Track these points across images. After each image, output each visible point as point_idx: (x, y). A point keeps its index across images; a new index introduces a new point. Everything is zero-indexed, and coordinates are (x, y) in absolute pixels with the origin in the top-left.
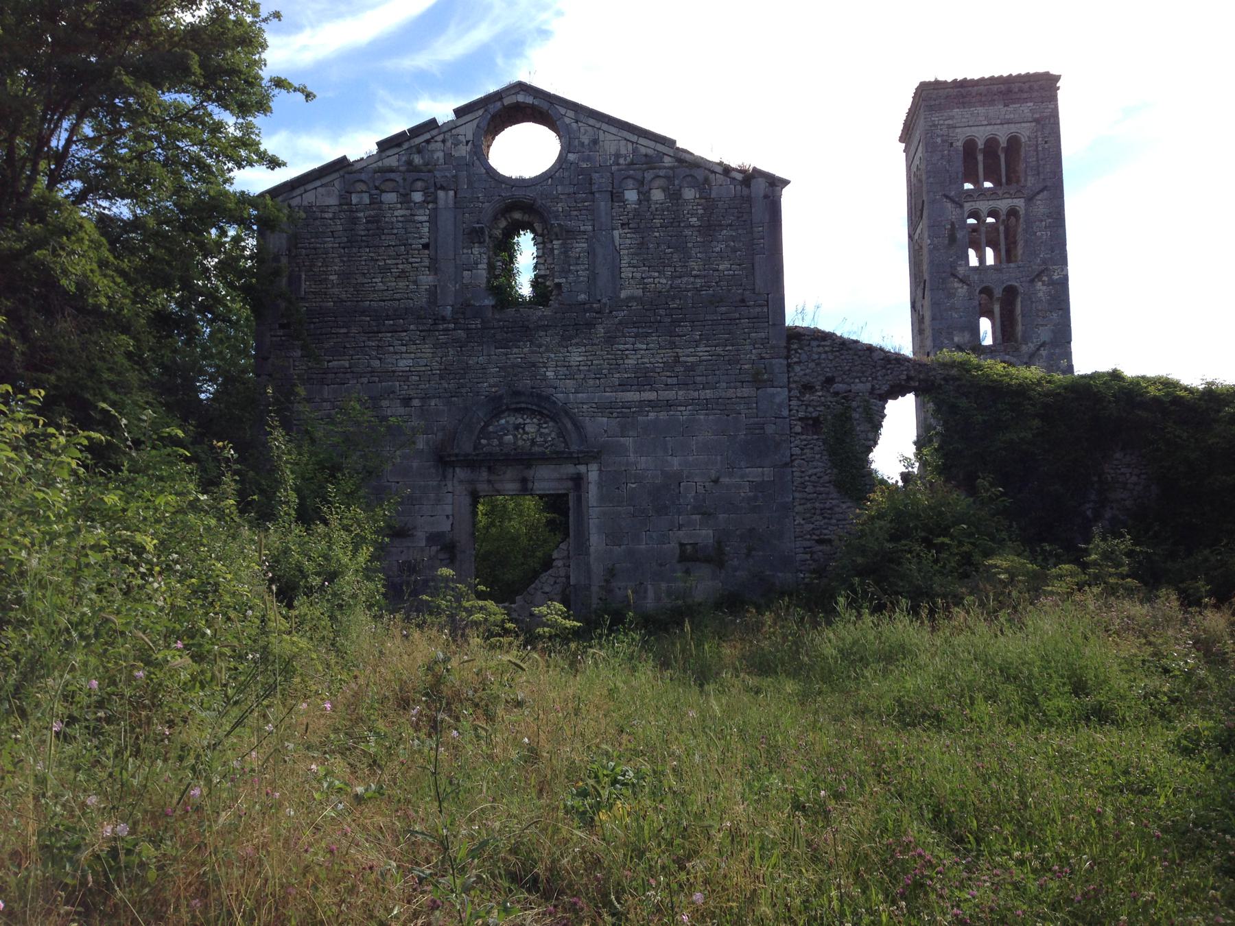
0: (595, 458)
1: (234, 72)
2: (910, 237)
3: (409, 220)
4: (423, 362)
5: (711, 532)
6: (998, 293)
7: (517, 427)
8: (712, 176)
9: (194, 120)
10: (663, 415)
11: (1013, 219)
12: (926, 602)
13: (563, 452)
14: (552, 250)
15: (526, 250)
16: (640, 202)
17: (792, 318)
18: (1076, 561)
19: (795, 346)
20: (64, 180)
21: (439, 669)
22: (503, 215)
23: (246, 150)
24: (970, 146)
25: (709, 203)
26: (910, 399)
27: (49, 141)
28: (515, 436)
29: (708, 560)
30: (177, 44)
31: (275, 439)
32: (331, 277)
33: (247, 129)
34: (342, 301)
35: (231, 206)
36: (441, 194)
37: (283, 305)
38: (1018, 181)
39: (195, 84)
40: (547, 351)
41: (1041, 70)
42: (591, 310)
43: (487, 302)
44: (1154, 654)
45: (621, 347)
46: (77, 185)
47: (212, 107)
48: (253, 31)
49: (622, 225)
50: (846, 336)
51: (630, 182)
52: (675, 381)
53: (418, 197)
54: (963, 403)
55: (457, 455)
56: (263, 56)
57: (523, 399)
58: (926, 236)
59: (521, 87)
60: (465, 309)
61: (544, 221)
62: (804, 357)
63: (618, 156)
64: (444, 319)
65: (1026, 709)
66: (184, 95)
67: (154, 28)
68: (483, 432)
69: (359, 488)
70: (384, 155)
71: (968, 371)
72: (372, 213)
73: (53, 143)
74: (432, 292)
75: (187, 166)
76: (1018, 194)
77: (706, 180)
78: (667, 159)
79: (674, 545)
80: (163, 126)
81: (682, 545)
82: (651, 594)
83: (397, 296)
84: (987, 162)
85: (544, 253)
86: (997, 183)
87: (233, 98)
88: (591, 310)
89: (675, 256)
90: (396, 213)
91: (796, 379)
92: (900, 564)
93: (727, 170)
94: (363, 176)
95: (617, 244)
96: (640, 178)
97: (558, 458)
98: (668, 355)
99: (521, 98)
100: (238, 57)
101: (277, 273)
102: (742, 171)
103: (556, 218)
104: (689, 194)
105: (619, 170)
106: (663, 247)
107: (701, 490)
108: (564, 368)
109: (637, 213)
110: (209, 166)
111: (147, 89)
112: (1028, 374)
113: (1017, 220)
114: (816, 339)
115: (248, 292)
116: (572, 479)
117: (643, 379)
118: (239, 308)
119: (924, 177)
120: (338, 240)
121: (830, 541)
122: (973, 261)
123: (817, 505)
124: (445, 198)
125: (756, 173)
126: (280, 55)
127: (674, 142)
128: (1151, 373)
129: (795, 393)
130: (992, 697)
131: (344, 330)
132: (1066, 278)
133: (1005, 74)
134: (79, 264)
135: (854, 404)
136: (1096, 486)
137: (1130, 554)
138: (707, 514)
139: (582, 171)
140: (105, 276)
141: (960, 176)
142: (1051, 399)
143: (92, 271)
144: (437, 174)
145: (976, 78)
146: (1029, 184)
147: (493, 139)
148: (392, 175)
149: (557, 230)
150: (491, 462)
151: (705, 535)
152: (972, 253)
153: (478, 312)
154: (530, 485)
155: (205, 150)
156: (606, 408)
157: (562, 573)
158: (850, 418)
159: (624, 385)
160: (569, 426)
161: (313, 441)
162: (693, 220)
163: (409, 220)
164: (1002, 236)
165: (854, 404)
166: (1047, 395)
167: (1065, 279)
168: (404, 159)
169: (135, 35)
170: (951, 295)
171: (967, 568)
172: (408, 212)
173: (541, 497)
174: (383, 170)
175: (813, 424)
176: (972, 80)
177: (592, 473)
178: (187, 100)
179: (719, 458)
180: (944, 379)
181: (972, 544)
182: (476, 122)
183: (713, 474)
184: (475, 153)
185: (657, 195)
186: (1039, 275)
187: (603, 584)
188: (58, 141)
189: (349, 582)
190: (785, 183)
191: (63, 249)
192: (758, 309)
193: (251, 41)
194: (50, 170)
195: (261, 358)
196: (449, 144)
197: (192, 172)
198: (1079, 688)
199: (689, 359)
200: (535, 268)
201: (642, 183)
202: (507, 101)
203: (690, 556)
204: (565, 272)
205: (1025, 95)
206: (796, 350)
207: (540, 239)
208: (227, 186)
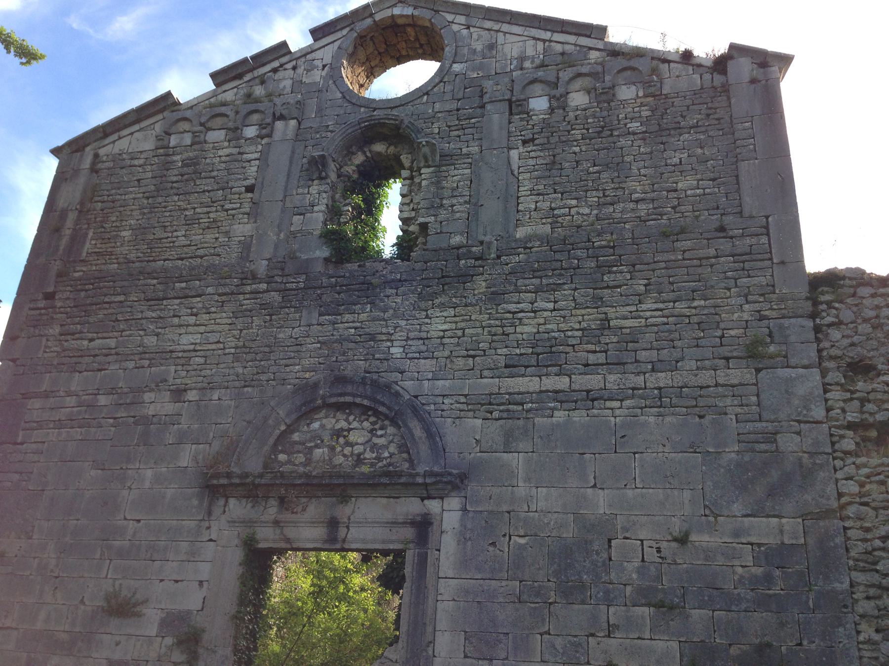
0: (456, 487)
4: (213, 338)
5: (675, 645)
7: (338, 433)
10: (579, 417)
13: (400, 475)
16: (552, 110)
17: (822, 251)
19: (827, 297)
22: (361, 149)
28: (332, 449)
32: (124, 234)
36: (279, 125)
40: (395, 316)
42: (469, 256)
45: (512, 307)
51: (538, 88)
53: (251, 132)
62: (847, 315)
64: (254, 277)
74: (246, 246)
83: (201, 252)
85: (410, 191)
88: (469, 256)
90: (220, 153)
91: (834, 352)
94: (188, 114)
95: (515, 167)
96: (552, 78)
98: (590, 318)
104: (626, 93)
106: (585, 165)
107: (651, 555)
116: (413, 523)
117: (546, 355)
120: (142, 190)
129: (836, 376)
131: (122, 298)
144: (278, 101)
148: (223, 110)
149: (426, 150)
153: (304, 268)
154: (342, 532)
156: (484, 405)
159: (512, 367)
160: (418, 432)
162: (634, 126)
163: (237, 159)
168: (242, 92)
177: (449, 513)
179: (687, 494)
182: (337, 44)
184: (332, 77)
185: (578, 99)
190: (785, 60)
196: (300, 71)
206: (829, 304)
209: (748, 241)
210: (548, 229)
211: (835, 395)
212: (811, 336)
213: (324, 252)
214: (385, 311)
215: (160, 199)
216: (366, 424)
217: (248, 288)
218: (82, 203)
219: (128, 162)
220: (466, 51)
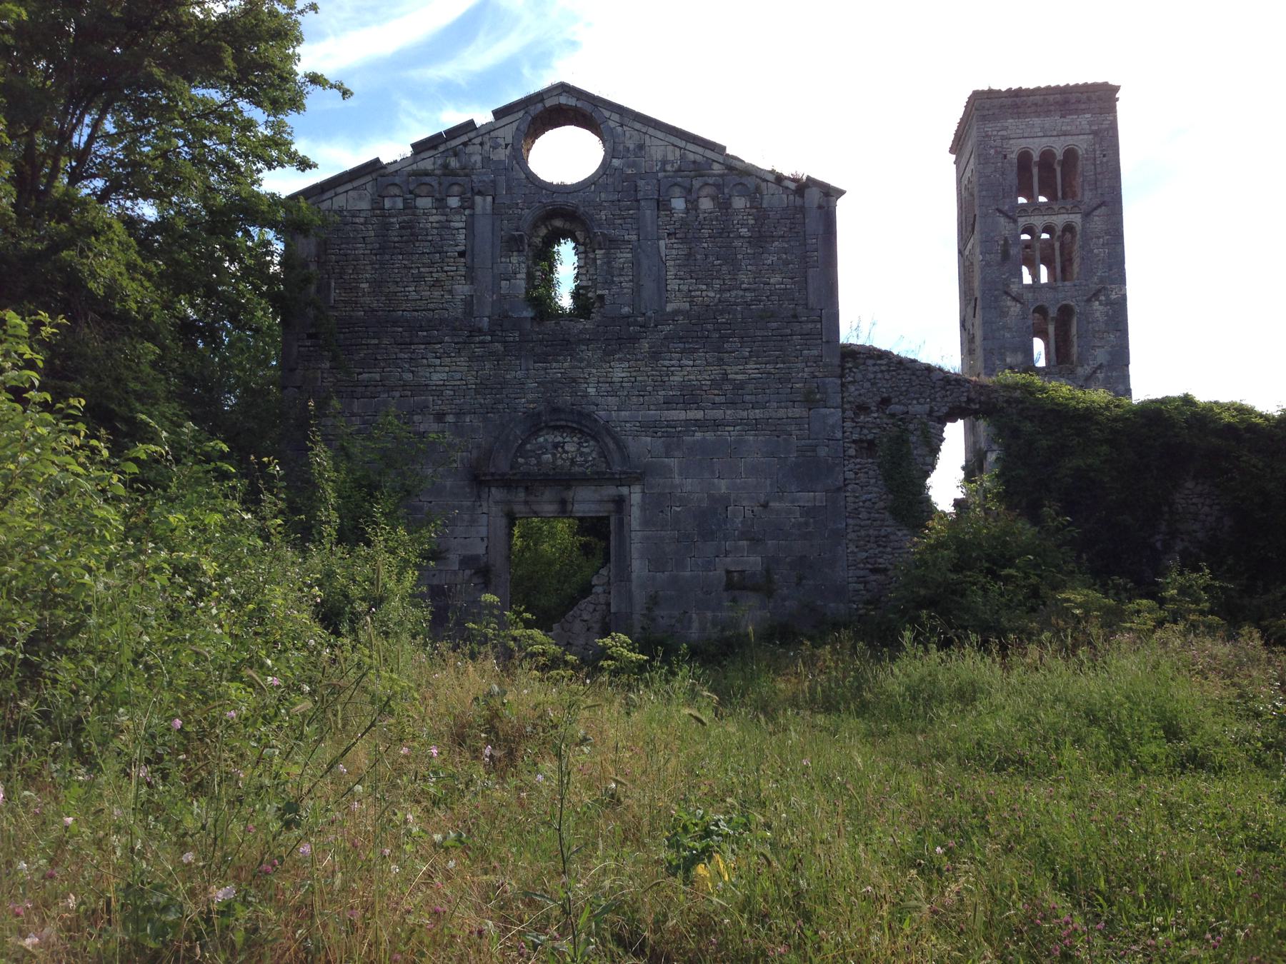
1: (268, 66)
2: (960, 252)
3: (445, 226)
4: (458, 376)
5: (759, 559)
6: (1053, 312)
7: (556, 446)
8: (764, 185)
9: (223, 117)
10: (710, 436)
11: (1068, 235)
12: (996, 637)
13: (604, 473)
14: (595, 260)
15: (567, 259)
16: (687, 211)
17: (847, 335)
18: (1151, 596)
19: (850, 365)
20: (87, 178)
21: (496, 703)
23: (277, 150)
24: (1025, 157)
25: (761, 214)
26: (960, 423)
27: (71, 137)
28: (554, 455)
29: (755, 589)
30: (207, 36)
31: (317, 455)
32: (363, 285)
33: (278, 127)
34: (373, 310)
35: (264, 208)
36: (478, 199)
37: (311, 312)
38: (1074, 195)
39: (228, 79)
40: (589, 365)
41: (1100, 80)
42: (636, 323)
43: (525, 314)
44: (1240, 696)
45: (666, 363)
46: (99, 183)
47: (242, 104)
48: (288, 24)
49: (669, 234)
50: (903, 355)
52: (722, 399)
53: (454, 202)
54: (1027, 426)
55: (492, 474)
56: (298, 50)
57: (563, 416)
58: (978, 250)
59: (563, 88)
60: (502, 322)
61: (587, 230)
62: (859, 376)
63: (664, 162)
64: (480, 330)
65: (1116, 755)
66: (212, 91)
67: (184, 19)
68: (521, 451)
69: (397, 507)
70: (419, 158)
71: (1032, 393)
72: (406, 218)
73: (75, 139)
74: (468, 302)
75: (213, 165)
76: (1075, 208)
77: (758, 189)
78: (716, 166)
79: (720, 572)
80: (190, 123)
81: (728, 572)
82: (695, 625)
83: (431, 306)
84: (1042, 176)
86: (1052, 197)
87: (266, 94)
88: (636, 323)
89: (724, 268)
90: (431, 219)
92: (963, 595)
93: (779, 178)
94: (397, 180)
95: (663, 255)
97: (598, 479)
98: (716, 372)
99: (563, 100)
100: (269, 50)
101: (307, 280)
102: (794, 180)
103: (600, 226)
104: (739, 203)
105: (666, 177)
107: (749, 514)
108: (606, 384)
109: (684, 223)
110: (239, 166)
111: (179, 83)
112: (1095, 397)
113: (1074, 236)
114: (871, 357)
115: (277, 301)
116: (613, 501)
117: (689, 397)
118: (265, 315)
119: (976, 190)
120: (369, 247)
121: (886, 570)
122: (1027, 279)
123: (871, 532)
124: (483, 204)
125: (811, 182)
126: (310, 58)
127: (724, 148)
128: (1224, 399)
129: (850, 414)
130: (1078, 741)
131: (376, 341)
132: (1124, 298)
133: (1062, 85)
134: (106, 266)
135: (911, 427)
136: (1166, 516)
137: (1206, 589)
138: (755, 541)
139: (628, 178)
140: (133, 279)
141: (1014, 189)
142: (1120, 425)
143: (120, 274)
145: (1032, 87)
146: (1086, 200)
147: (533, 142)
148: (427, 179)
150: (529, 482)
151: (753, 562)
152: (1025, 270)
154: (569, 507)
155: (233, 149)
156: (650, 427)
157: (602, 599)
158: (906, 441)
159: (668, 403)
160: (612, 445)
161: (349, 457)
162: (744, 231)
163: (445, 226)
164: (1057, 253)
165: (911, 427)
166: (1116, 420)
167: (1124, 299)
168: (439, 162)
169: (165, 25)
170: (1004, 314)
171: (1035, 600)
172: (443, 218)
173: (581, 519)
174: (417, 174)
175: (868, 447)
176: (1027, 90)
177: (635, 495)
178: (216, 96)
180: (1007, 401)
181: (1038, 575)
182: (515, 125)
183: (762, 498)
184: (515, 157)
185: (706, 204)
186: (1096, 295)
187: (645, 612)
188: (80, 138)
189: (395, 608)
190: (841, 193)
191: (90, 250)
192: (810, 326)
193: (286, 34)
194: (71, 167)
195: (287, 366)
196: (487, 147)
197: (219, 172)
198: (1172, 732)
199: (739, 377)
200: (576, 278)
201: (690, 191)
202: (548, 103)
203: (736, 584)
204: (609, 283)
205: (1083, 106)
207: (581, 248)
208: (255, 188)
211: (848, 424)
215: (387, 257)
218: (318, 256)
220: (621, 147)
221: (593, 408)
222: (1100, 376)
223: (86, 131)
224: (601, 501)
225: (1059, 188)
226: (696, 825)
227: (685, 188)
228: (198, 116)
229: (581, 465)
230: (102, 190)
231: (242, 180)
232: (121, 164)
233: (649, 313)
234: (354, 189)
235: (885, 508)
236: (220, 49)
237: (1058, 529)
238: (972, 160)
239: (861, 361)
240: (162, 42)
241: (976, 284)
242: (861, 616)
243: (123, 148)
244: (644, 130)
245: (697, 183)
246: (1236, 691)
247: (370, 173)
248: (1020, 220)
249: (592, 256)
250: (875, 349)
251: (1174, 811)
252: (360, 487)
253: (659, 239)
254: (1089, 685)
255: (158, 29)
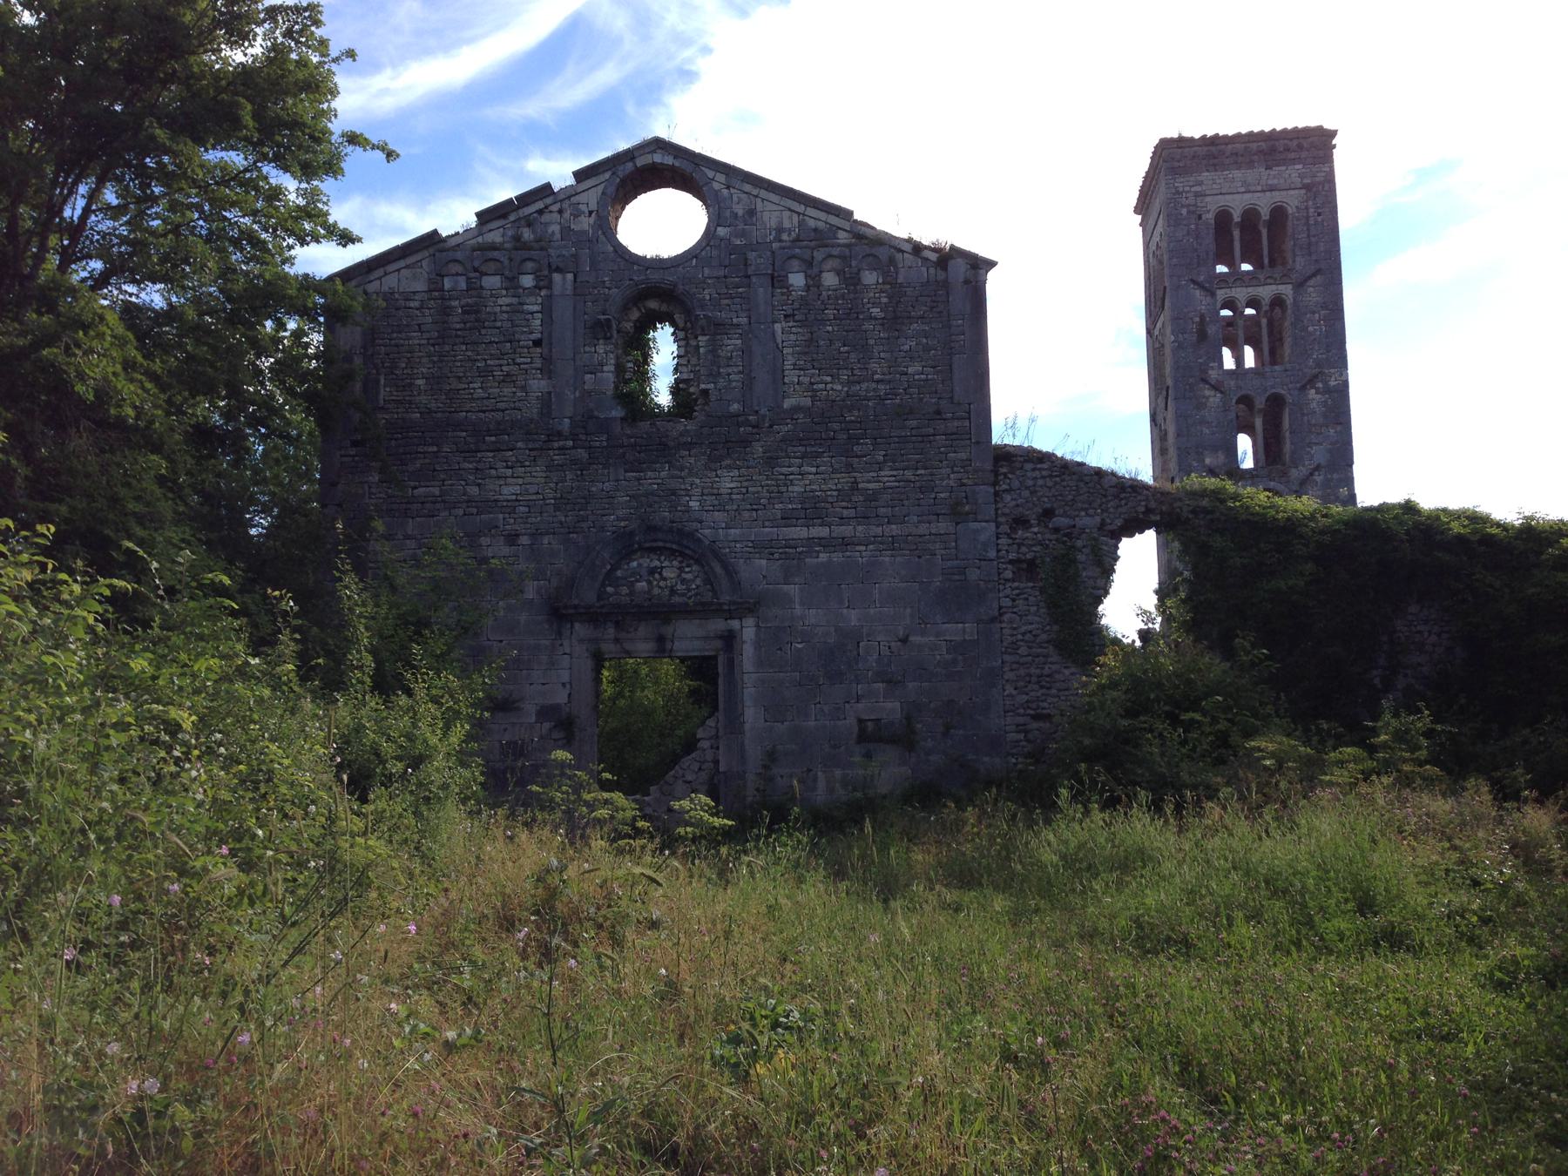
1: (296, 124)
2: (1149, 332)
3: (516, 310)
4: (533, 489)
6: (1260, 403)
7: (652, 571)
9: (245, 184)
10: (837, 557)
11: (1277, 310)
12: (1172, 795)
14: (698, 347)
15: (664, 348)
16: (808, 288)
17: (1000, 435)
18: (1361, 743)
19: (1004, 470)
21: (554, 880)
22: (635, 304)
23: (311, 222)
24: (1223, 217)
26: (1150, 536)
27: (61, 210)
28: (649, 582)
30: (224, 90)
31: (346, 587)
33: (313, 196)
34: (430, 411)
36: (557, 277)
38: (1284, 264)
39: (247, 140)
40: (691, 474)
41: (1313, 123)
42: (747, 423)
44: (1461, 862)
45: (784, 470)
46: (97, 265)
47: (267, 169)
48: (320, 74)
50: (1068, 457)
51: (795, 263)
52: (852, 513)
53: (527, 281)
55: (576, 607)
56: (333, 104)
57: (660, 535)
58: (1168, 330)
59: (658, 144)
61: (688, 312)
62: (1016, 484)
64: (559, 434)
66: (233, 154)
67: (196, 69)
70: (485, 228)
71: (1223, 501)
73: (67, 213)
74: (546, 401)
75: (236, 243)
77: (892, 261)
78: (841, 234)
79: (851, 721)
81: (860, 721)
82: (821, 784)
83: (502, 405)
84: (1245, 238)
86: (1258, 265)
88: (747, 423)
90: (500, 301)
93: (917, 248)
94: (459, 255)
95: (779, 341)
96: (807, 257)
97: (703, 610)
98: (844, 480)
99: (658, 158)
100: (302, 106)
102: (936, 250)
103: (703, 307)
104: (870, 278)
108: (713, 498)
110: (264, 242)
111: (186, 146)
112: (1298, 506)
114: (1029, 461)
115: (311, 398)
116: (721, 637)
117: (812, 510)
118: (300, 421)
122: (1229, 362)
123: (1033, 671)
124: (562, 282)
125: (955, 252)
127: (850, 213)
128: (1454, 505)
129: (1005, 528)
130: (1255, 916)
132: (1346, 384)
134: (98, 366)
135: (1079, 543)
137: (1429, 734)
140: (132, 380)
142: (1327, 538)
146: (1298, 267)
148: (495, 254)
150: (621, 616)
151: (891, 709)
154: (668, 646)
156: (764, 547)
157: (709, 756)
159: (787, 519)
160: (718, 569)
161: (393, 589)
163: (516, 310)
164: (1265, 331)
165: (1079, 543)
166: (1322, 532)
168: (510, 233)
169: (172, 77)
170: (1201, 406)
171: (1223, 752)
173: (683, 660)
174: (482, 248)
175: (1028, 568)
176: (1226, 137)
177: (748, 630)
178: (237, 159)
180: (1193, 512)
181: (1228, 720)
184: (600, 226)
185: (830, 279)
186: (1311, 382)
188: (73, 211)
189: (439, 769)
190: (991, 264)
191: (78, 346)
193: (318, 86)
196: (567, 215)
197: (242, 250)
198: (1365, 905)
200: (676, 370)
202: (640, 162)
203: (871, 736)
205: (1292, 155)
207: (681, 334)
208: (287, 268)
209: (956, 424)
210: (808, 402)
211: (1004, 541)
212: (992, 499)
213: (618, 413)
214: (682, 470)
215: (447, 348)
216: (675, 563)
217: (556, 445)
218: (364, 347)
219: (402, 303)
220: (728, 213)
221: (696, 525)
222: (1318, 478)
223: (81, 203)
224: (706, 638)
225: (1266, 252)
226: (766, 1017)
227: (804, 261)
228: (217, 183)
229: (683, 595)
230: (102, 273)
231: (268, 258)
232: (124, 240)
233: (763, 411)
234: (407, 267)
235: (1048, 642)
236: (238, 105)
237: (1253, 665)
238: (1160, 222)
239: (1018, 465)
240: (169, 98)
241: (1168, 370)
242: (1020, 771)
243: (128, 223)
244: (755, 192)
245: (819, 255)
246: (1456, 856)
247: (426, 248)
248: (1219, 292)
249: (693, 343)
250: (1034, 451)
251: (1349, 996)
252: (407, 623)
253: (774, 322)
254: (1278, 850)
255: (164, 83)
